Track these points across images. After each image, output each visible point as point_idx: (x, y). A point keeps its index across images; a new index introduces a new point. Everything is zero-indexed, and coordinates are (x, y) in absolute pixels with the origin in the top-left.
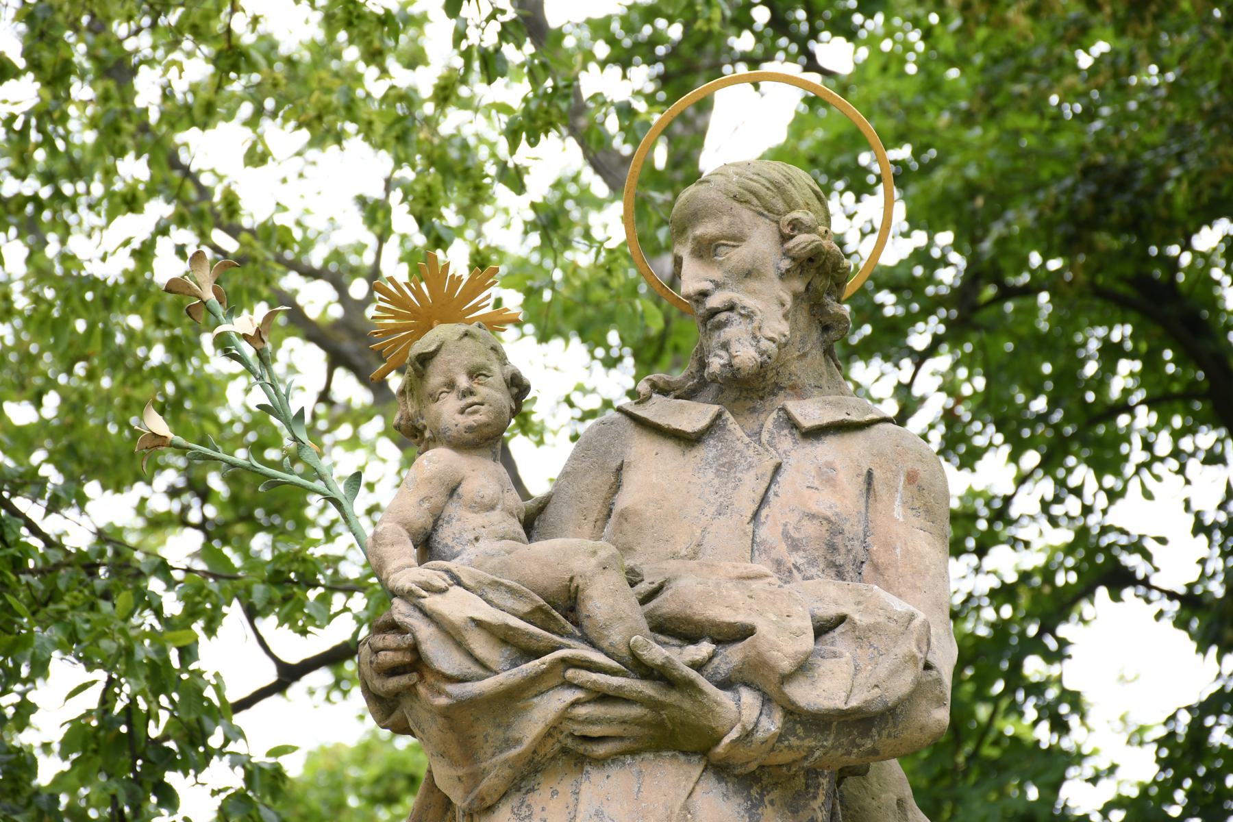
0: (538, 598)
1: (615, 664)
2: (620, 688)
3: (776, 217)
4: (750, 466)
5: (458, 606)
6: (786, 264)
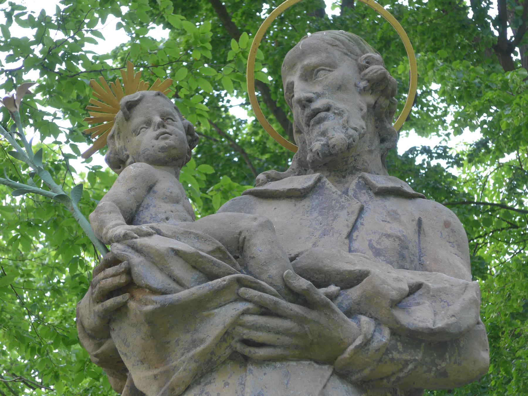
0: (217, 242)
3: (355, 57)
6: (363, 84)
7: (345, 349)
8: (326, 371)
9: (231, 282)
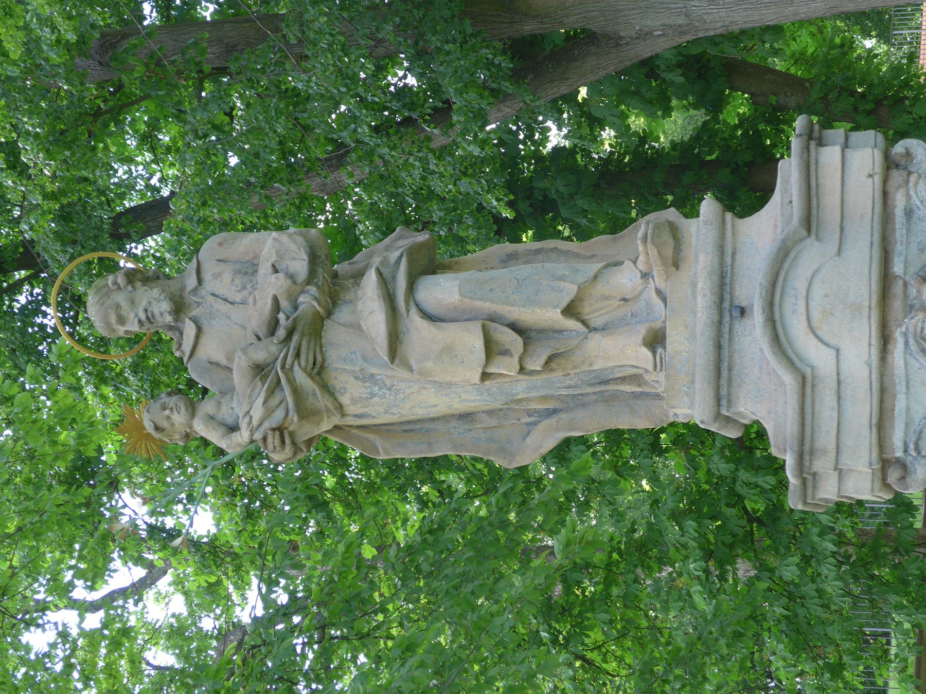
1: (285, 350)
2: (294, 348)
4: (211, 306)
5: (257, 412)
7: (319, 312)
8: (328, 322)
9: (284, 373)
